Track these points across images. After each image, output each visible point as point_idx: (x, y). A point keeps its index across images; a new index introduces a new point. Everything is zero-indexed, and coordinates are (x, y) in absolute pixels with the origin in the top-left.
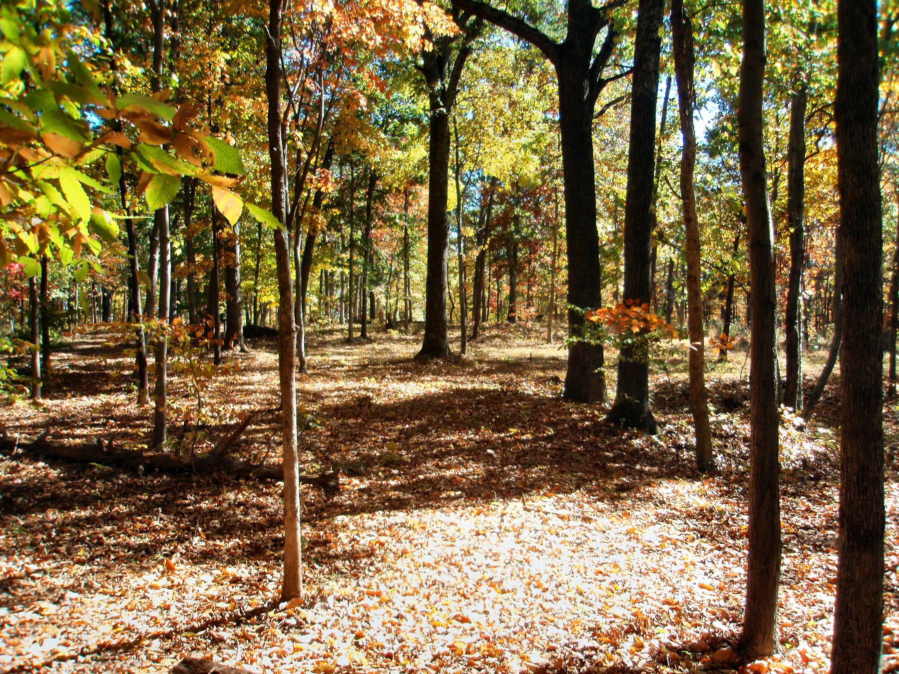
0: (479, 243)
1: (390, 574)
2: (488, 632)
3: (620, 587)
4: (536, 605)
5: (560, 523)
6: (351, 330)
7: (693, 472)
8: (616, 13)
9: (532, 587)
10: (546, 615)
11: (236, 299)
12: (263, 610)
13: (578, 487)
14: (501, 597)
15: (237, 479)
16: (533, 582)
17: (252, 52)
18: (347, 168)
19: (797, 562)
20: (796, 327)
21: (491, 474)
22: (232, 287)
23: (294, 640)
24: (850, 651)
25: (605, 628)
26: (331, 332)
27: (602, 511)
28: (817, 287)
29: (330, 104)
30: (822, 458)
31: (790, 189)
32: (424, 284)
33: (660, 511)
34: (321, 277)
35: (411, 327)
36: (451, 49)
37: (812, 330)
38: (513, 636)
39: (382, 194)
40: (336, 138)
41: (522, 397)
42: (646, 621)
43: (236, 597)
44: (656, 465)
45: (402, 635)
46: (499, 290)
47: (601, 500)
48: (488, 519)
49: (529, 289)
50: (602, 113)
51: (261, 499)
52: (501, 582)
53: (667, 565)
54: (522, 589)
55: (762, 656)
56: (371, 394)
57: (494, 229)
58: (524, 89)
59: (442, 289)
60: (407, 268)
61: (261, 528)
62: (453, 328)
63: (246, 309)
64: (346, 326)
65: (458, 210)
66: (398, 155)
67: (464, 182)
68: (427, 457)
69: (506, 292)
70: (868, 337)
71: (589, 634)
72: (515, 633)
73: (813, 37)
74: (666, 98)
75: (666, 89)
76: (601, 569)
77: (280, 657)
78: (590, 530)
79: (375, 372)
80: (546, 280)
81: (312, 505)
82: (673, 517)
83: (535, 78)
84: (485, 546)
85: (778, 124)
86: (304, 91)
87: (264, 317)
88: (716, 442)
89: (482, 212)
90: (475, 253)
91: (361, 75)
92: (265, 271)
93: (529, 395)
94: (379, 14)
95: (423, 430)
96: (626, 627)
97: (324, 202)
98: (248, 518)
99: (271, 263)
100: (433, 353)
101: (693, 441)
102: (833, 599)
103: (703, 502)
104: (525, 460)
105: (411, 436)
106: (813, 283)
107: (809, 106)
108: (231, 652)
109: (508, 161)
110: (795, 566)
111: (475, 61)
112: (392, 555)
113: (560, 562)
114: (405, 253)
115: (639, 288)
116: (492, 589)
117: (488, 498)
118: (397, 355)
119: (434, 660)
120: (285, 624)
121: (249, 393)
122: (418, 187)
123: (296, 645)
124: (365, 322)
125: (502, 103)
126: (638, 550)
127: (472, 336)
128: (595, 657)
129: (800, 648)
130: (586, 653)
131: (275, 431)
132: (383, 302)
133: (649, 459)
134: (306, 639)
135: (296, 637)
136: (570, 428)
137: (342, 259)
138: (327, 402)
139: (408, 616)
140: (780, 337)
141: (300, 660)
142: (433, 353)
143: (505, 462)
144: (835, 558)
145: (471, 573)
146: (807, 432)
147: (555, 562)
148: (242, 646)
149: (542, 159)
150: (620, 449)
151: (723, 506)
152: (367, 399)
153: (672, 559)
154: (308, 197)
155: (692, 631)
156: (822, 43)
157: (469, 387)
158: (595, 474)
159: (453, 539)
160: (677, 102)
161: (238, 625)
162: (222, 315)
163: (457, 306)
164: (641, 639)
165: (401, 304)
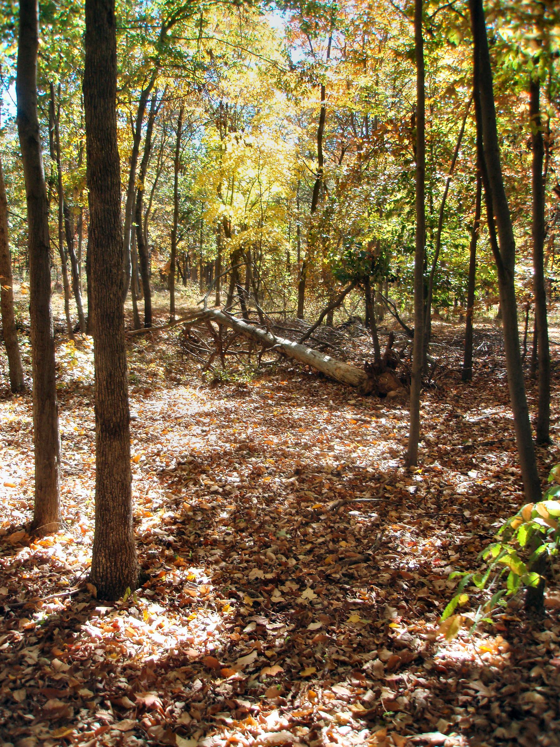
19: (85, 457)
55: (50, 533)
70: (111, 271)
103: (13, 418)
129: (81, 523)
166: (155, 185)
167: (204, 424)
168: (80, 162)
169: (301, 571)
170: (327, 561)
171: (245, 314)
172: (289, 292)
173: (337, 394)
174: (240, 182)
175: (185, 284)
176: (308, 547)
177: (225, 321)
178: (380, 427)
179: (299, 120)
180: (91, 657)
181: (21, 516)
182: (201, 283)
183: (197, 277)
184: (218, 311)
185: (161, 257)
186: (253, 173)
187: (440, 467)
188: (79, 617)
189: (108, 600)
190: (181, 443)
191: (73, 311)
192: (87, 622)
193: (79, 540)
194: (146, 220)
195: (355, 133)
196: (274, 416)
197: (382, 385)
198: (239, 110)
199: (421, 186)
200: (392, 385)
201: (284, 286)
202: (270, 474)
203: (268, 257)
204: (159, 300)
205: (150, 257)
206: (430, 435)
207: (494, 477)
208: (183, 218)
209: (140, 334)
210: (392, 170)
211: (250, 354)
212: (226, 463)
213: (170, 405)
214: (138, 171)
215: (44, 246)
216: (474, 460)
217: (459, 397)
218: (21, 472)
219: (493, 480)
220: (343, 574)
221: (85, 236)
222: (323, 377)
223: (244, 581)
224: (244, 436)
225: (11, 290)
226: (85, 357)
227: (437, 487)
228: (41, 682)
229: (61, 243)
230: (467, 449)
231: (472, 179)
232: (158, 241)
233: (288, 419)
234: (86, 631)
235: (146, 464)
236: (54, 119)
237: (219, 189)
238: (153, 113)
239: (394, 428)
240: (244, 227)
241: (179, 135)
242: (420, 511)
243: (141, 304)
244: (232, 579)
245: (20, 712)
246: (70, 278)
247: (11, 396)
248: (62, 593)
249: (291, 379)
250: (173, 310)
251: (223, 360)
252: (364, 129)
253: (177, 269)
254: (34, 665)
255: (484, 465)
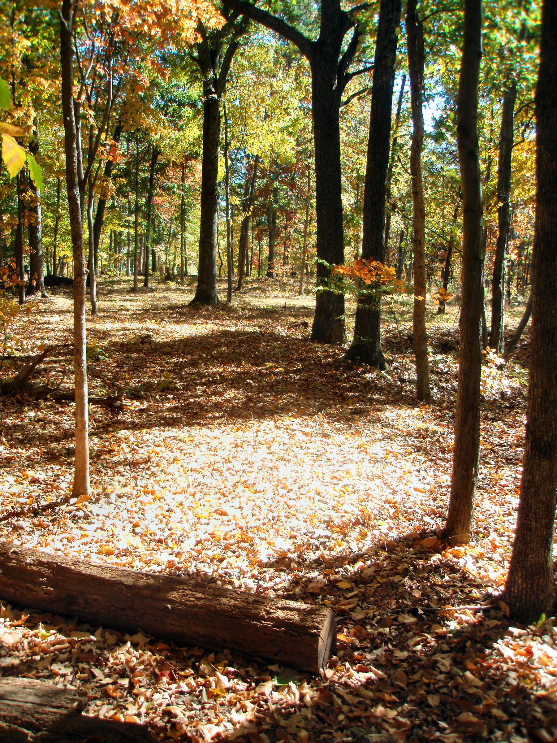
0: (244, 211)
1: (162, 476)
2: (242, 523)
3: (350, 489)
4: (283, 502)
5: (305, 438)
6: (135, 281)
7: (414, 400)
8: (362, 16)
9: (279, 488)
10: (290, 510)
11: (37, 253)
12: (56, 504)
13: (320, 410)
14: (254, 496)
15: (37, 399)
16: (280, 484)
17: (49, 39)
18: (133, 144)
20: (500, 286)
21: (249, 399)
22: (34, 242)
23: (81, 528)
24: (529, 538)
25: (337, 521)
26: (119, 282)
27: (338, 430)
28: (519, 255)
29: (117, 88)
30: (518, 392)
31: (500, 172)
32: (197, 244)
33: (385, 430)
34: (111, 236)
35: (186, 280)
36: (222, 43)
37: (514, 290)
38: (262, 526)
39: (164, 167)
40: (124, 115)
41: (277, 338)
42: (370, 516)
43: (34, 494)
44: (384, 394)
45: (171, 525)
46: (260, 251)
47: (338, 421)
48: (245, 434)
49: (285, 250)
50: (348, 101)
51: (57, 417)
52: (254, 484)
53: (389, 473)
54: (271, 490)
55: (460, 543)
56: (151, 333)
57: (256, 199)
58: (284, 81)
59: (212, 248)
60: (184, 230)
61: (57, 439)
62: (221, 281)
63: (47, 262)
64: (131, 278)
65: (226, 179)
66: (177, 134)
67: (231, 159)
68: (197, 385)
69: (266, 252)
71: (324, 526)
72: (264, 524)
73: (524, 43)
74: (402, 92)
75: (401, 84)
76: (336, 475)
77: (70, 542)
78: (328, 445)
79: (155, 316)
80: (299, 242)
81: (100, 421)
82: (396, 435)
83: (293, 72)
84: (242, 456)
85: (493, 118)
86: (95, 75)
87: (62, 269)
88: (433, 377)
89: (247, 185)
90: (241, 219)
91: (144, 63)
92: (62, 230)
93: (282, 336)
94: (158, 9)
95: (194, 364)
96: (353, 521)
97: (114, 172)
98: (46, 432)
99: (66, 222)
100: (204, 300)
101: (415, 377)
102: (518, 501)
103: (420, 425)
104: (276, 388)
105: (184, 368)
106: (516, 251)
107: (518, 102)
108: (28, 537)
109: (267, 141)
110: (491, 475)
111: (242, 55)
112: (165, 462)
113: (303, 469)
114: (182, 219)
115: (375, 248)
116: (247, 489)
117: (246, 418)
118: (174, 302)
119: (197, 544)
120: (75, 516)
121: (48, 330)
122: (193, 162)
123: (83, 533)
124: (146, 273)
125: (264, 91)
126: (366, 461)
127: (236, 287)
128: (328, 544)
129: (491, 538)
130: (321, 540)
131: (69, 362)
132: (163, 258)
133: (380, 390)
134: (92, 527)
135: (84, 526)
136: (315, 363)
137: (129, 222)
138: (114, 339)
139: (176, 509)
140: (488, 295)
141: (86, 544)
142: (204, 300)
143: (261, 389)
144: (521, 469)
145: (230, 478)
146: (506, 372)
147: (299, 469)
148: (37, 533)
149: (297, 140)
150: (356, 381)
151: (436, 428)
152: (148, 336)
153: (393, 468)
154: (99, 167)
155: (406, 524)
156: (531, 50)
157: (233, 329)
158: (334, 400)
159: (215, 450)
160: (409, 95)
161: (35, 516)
162: (26, 266)
163: (225, 263)
164: (366, 529)
165: (178, 261)
180: (504, 676)
181: (432, 522)
188: (491, 633)
189: (520, 622)
192: (499, 641)
193: (490, 555)
225: (424, 301)
228: (454, 692)
234: (498, 650)
245: (434, 717)
247: (417, 403)
248: (473, 606)
254: (446, 673)
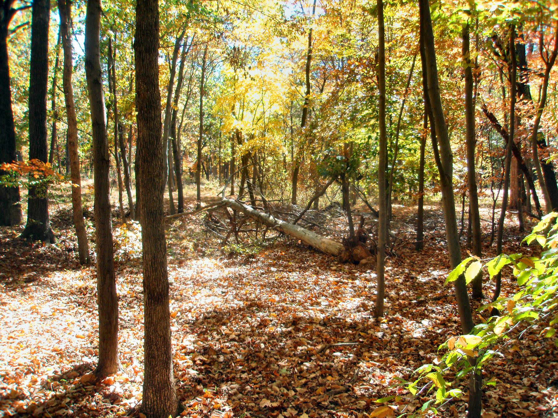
103: (81, 284)
129: (133, 365)
166: (185, 106)
167: (224, 287)
168: (131, 89)
169: (298, 400)
170: (317, 392)
171: (253, 202)
172: (286, 184)
173: (322, 262)
174: (248, 103)
175: (208, 178)
176: (303, 381)
177: (237, 207)
178: (354, 287)
179: (292, 57)
182: (220, 178)
183: (216, 173)
184: (232, 200)
185: (190, 159)
186: (258, 97)
187: (400, 317)
190: (205, 301)
191: (125, 201)
193: (133, 379)
194: (179, 132)
195: (333, 66)
196: (276, 280)
197: (355, 255)
198: (248, 51)
199: (382, 106)
200: (364, 254)
201: (282, 179)
202: (274, 325)
203: (270, 158)
204: (189, 191)
205: (182, 159)
206: (393, 293)
207: (441, 324)
208: (206, 130)
209: (176, 218)
210: (360, 94)
211: (257, 231)
212: (241, 317)
213: (198, 273)
214: (173, 96)
215: (104, 159)
216: (426, 312)
217: (414, 263)
218: (88, 327)
219: (441, 327)
220: (330, 402)
221: (134, 143)
222: (313, 250)
223: (255, 409)
224: (253, 296)
226: (134, 236)
227: (399, 333)
229: (116, 150)
230: (420, 303)
231: (420, 101)
232: (188, 147)
233: (286, 282)
235: (180, 319)
236: (111, 61)
237: (233, 108)
238: (184, 53)
239: (365, 287)
240: (252, 137)
241: (204, 70)
242: (385, 352)
243: (175, 194)
244: (247, 407)
246: (123, 176)
249: (287, 250)
250: (199, 199)
251: (236, 235)
252: (341, 63)
253: (202, 167)
255: (434, 315)
